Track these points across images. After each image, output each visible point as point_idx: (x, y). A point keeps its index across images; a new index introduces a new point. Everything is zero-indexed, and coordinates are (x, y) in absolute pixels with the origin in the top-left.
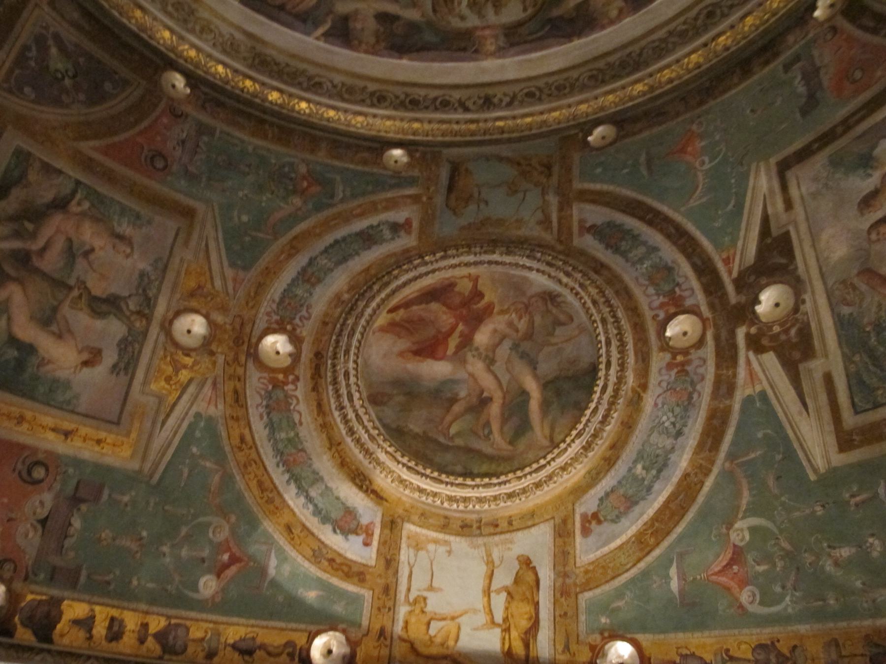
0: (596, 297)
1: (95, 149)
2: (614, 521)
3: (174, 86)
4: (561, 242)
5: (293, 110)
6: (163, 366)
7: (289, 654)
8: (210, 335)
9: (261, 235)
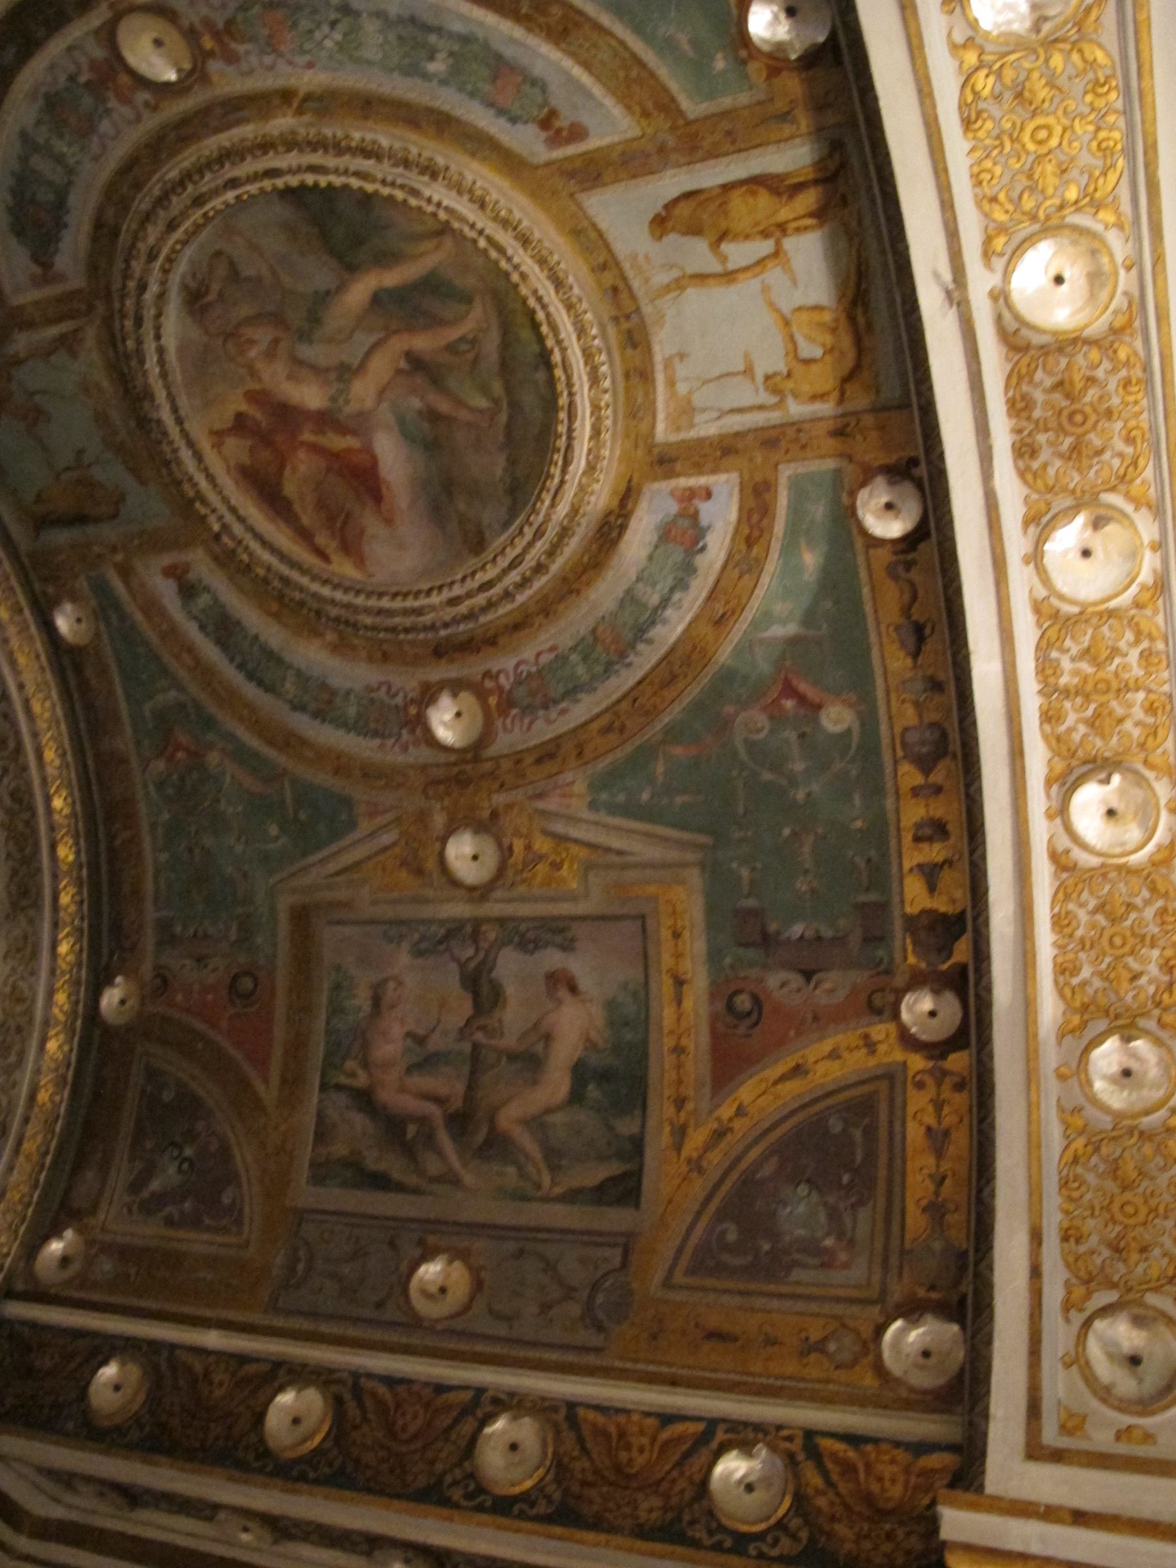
0: (161, 226)
1: (266, 1081)
2: (544, 89)
3: (123, 1002)
4: (91, 308)
5: (74, 814)
6: (539, 879)
7: (908, 570)
8: (467, 826)
9: (288, 794)
